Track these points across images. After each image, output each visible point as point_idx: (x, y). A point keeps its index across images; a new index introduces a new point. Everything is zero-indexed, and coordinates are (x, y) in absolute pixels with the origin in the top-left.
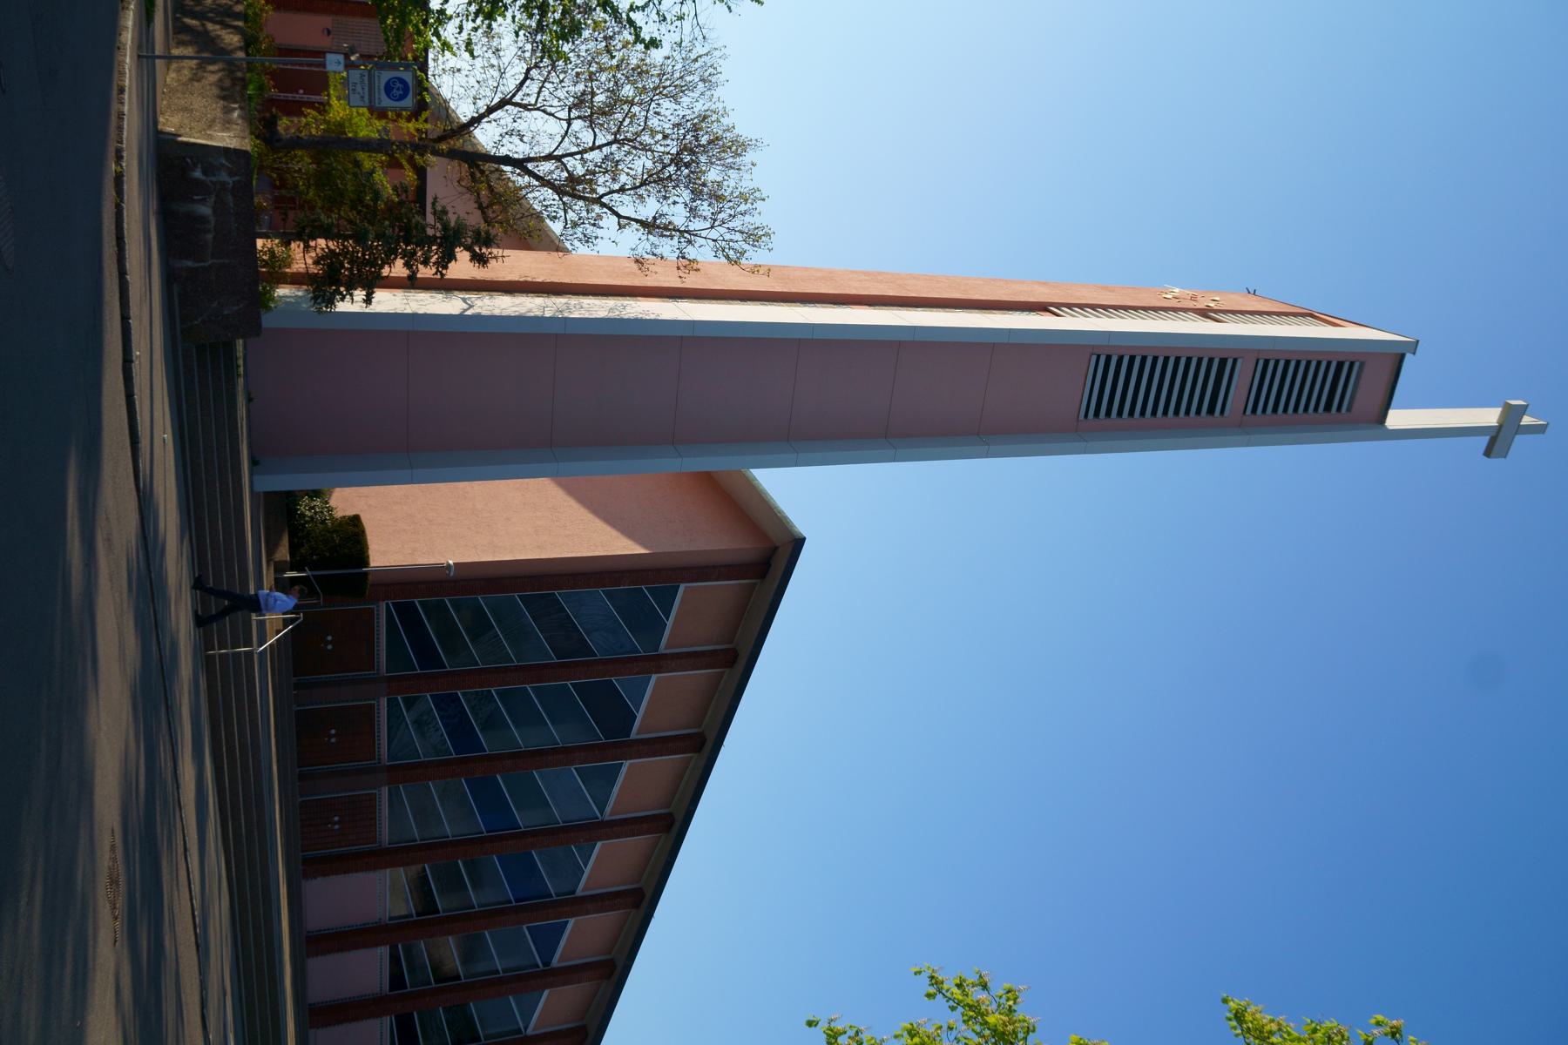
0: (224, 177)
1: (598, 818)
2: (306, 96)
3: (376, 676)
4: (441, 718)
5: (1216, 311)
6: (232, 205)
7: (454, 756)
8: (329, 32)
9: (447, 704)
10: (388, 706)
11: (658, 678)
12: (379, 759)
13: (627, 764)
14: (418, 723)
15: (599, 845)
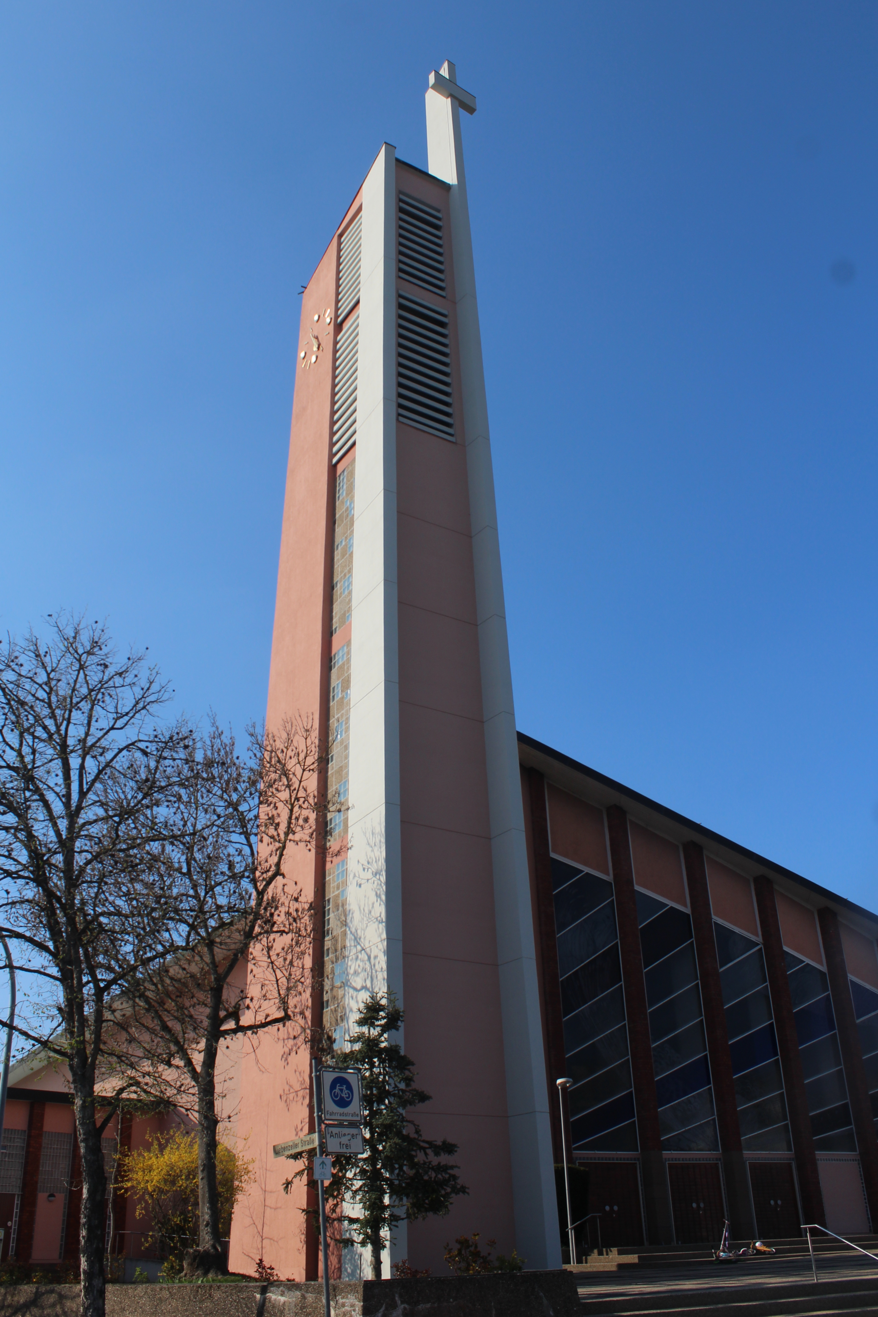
1: (761, 949)
5: (337, 317)
6: (428, 1305)
8: (52, 1195)
10: (670, 1150)
11: (637, 884)
12: (717, 1159)
15: (786, 948)
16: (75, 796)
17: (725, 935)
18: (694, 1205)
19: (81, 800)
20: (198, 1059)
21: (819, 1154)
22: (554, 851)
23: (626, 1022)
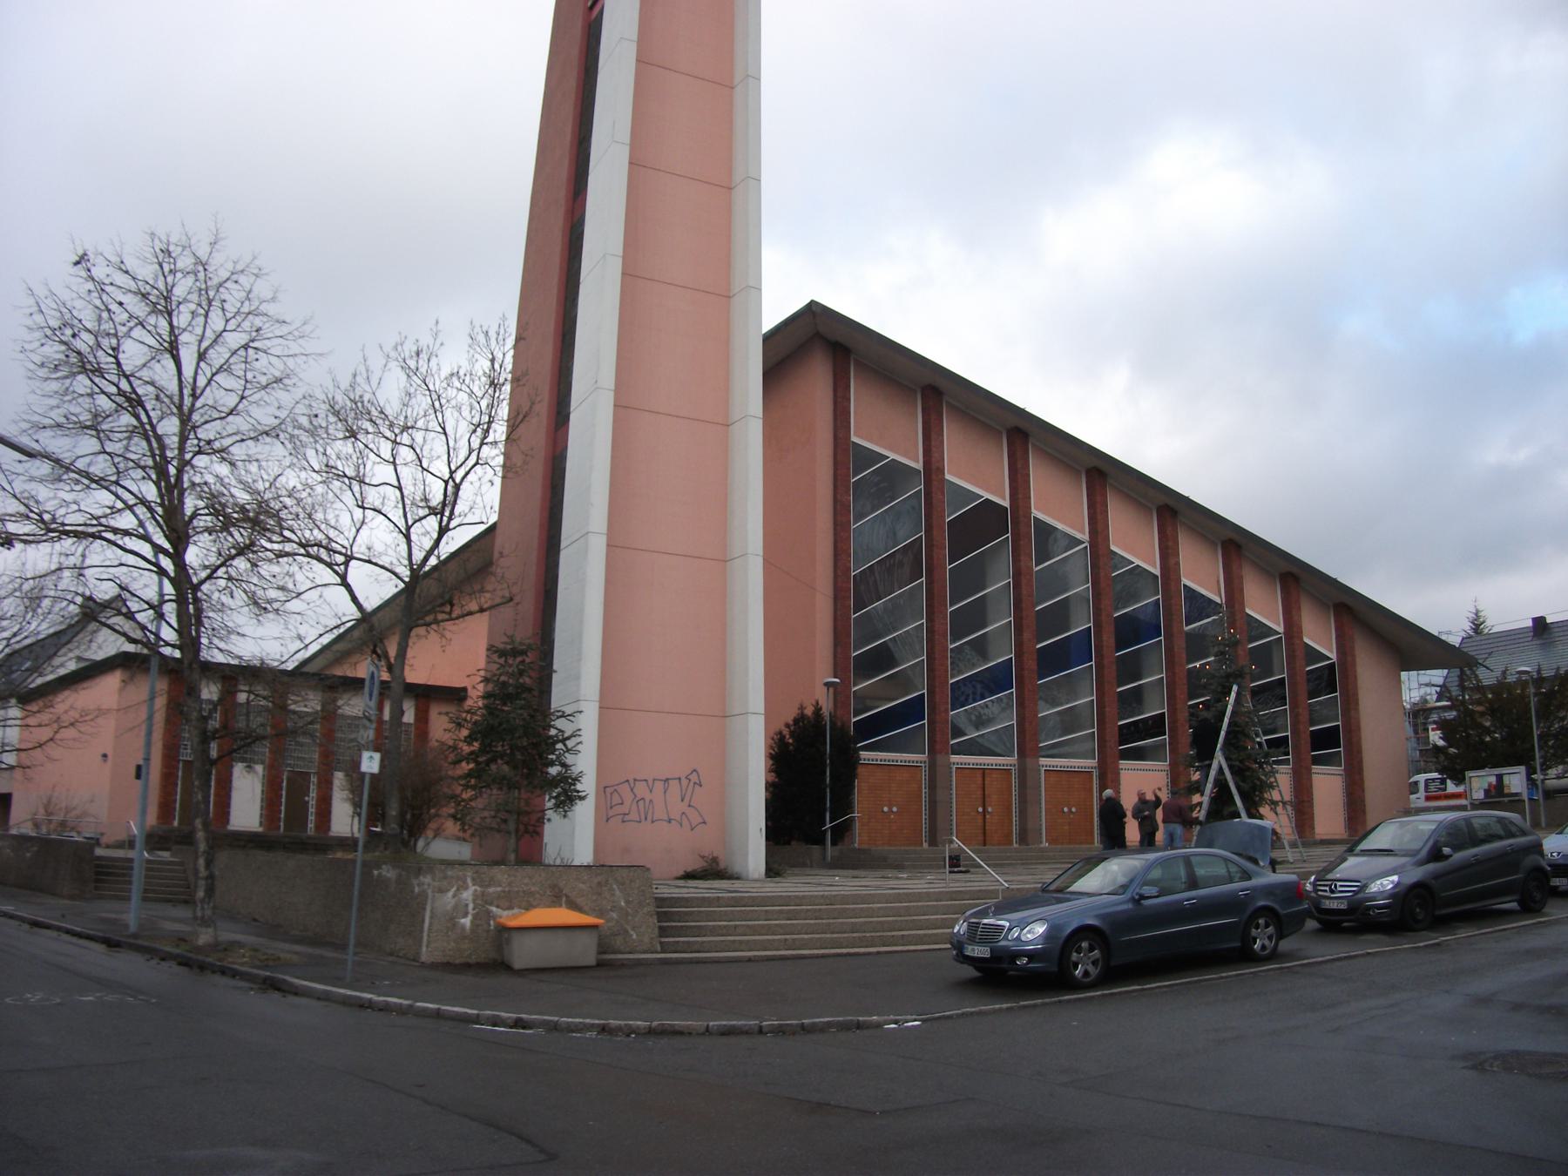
0: (467, 895)
3: (927, 765)
4: (975, 701)
9: (961, 695)
13: (1035, 513)
14: (980, 723)
15: (1113, 548)
16: (187, 401)
17: (1045, 531)
20: (392, 651)
21: (1123, 763)
23: (924, 620)
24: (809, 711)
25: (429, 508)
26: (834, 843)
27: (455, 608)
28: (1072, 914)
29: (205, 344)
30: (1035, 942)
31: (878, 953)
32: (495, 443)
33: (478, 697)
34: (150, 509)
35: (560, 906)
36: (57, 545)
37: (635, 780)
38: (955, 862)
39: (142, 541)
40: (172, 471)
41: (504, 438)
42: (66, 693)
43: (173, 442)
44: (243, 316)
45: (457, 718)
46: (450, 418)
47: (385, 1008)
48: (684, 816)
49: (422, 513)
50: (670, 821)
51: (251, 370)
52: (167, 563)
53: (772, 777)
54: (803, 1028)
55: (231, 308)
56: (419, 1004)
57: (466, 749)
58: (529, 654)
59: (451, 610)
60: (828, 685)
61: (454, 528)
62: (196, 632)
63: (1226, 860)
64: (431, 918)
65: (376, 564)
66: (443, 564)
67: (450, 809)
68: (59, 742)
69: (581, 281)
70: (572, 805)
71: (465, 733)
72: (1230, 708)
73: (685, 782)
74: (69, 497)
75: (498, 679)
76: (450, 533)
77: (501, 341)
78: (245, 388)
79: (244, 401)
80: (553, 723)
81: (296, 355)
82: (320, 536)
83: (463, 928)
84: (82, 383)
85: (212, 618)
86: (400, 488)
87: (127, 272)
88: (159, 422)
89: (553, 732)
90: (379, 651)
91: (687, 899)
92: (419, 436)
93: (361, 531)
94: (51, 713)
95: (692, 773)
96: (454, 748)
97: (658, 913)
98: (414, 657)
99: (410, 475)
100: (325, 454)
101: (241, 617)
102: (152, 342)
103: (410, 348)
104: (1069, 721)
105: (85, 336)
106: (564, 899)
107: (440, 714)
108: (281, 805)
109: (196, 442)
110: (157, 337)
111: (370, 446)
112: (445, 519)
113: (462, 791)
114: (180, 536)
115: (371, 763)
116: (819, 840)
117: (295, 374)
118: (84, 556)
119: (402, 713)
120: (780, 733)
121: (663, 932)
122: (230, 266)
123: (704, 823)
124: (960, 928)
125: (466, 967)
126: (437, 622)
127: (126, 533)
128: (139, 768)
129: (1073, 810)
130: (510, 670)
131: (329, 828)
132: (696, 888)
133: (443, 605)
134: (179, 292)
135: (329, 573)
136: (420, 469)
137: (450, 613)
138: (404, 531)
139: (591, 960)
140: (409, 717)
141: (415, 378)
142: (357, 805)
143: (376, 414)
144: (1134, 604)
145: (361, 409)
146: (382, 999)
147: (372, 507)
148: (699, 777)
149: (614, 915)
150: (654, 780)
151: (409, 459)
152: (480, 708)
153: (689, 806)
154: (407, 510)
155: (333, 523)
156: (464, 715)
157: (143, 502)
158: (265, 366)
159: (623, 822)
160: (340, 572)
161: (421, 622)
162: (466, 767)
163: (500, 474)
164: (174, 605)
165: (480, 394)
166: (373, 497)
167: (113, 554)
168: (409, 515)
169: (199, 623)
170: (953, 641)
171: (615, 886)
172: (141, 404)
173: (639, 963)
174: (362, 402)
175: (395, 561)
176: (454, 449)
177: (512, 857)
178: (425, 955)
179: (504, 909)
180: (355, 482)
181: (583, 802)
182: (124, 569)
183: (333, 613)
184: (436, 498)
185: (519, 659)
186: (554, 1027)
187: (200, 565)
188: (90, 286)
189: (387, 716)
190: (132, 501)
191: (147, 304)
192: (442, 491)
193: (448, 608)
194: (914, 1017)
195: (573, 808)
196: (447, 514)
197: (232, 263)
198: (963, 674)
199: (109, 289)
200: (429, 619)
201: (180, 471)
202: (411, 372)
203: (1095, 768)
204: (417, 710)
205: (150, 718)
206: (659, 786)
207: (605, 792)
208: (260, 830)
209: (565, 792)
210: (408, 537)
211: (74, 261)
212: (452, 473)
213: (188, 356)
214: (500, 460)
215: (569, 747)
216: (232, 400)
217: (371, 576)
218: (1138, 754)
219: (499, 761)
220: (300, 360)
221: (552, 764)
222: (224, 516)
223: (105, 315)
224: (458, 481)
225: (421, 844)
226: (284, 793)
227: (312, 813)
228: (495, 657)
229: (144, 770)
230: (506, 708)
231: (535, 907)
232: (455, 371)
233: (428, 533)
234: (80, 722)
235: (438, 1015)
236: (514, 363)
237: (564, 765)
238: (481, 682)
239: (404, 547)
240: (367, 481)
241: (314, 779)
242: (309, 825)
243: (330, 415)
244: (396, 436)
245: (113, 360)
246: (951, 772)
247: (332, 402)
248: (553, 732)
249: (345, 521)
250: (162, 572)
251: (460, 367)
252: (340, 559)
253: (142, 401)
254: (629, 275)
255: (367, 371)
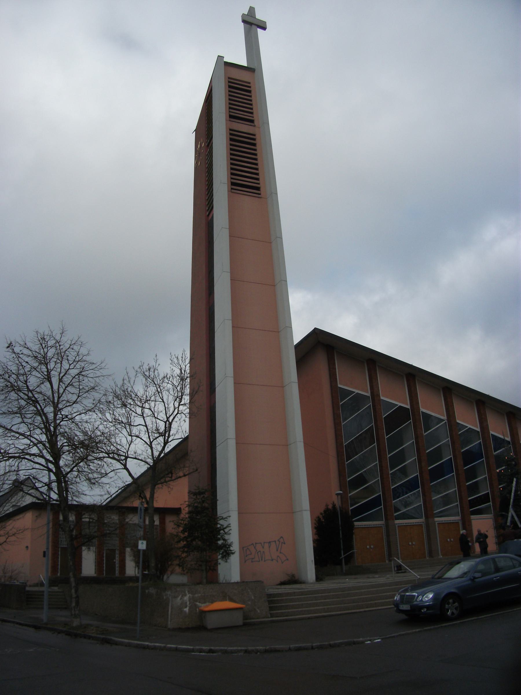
0: (186, 598)
1: (446, 422)
2: (116, 558)
4: (403, 495)
7: (420, 489)
9: (397, 493)
14: (406, 505)
15: (458, 421)
16: (56, 399)
17: (427, 417)
18: (368, 547)
19: (58, 401)
20: (148, 495)
21: (473, 517)
22: (340, 384)
24: (330, 507)
25: (159, 433)
26: (346, 564)
27: (173, 475)
28: (444, 588)
29: (62, 375)
30: (429, 601)
31: (365, 611)
32: (185, 404)
33: (186, 513)
34: (44, 445)
35: (226, 600)
36: (7, 463)
37: (256, 543)
38: (399, 568)
39: (41, 458)
40: (52, 429)
41: (188, 402)
42: (11, 522)
43: (51, 416)
44: (77, 362)
45: (177, 523)
46: (165, 395)
47: (155, 648)
48: (278, 558)
49: (157, 435)
50: (272, 560)
51: (81, 385)
52: (51, 466)
53: (316, 537)
54: (331, 646)
55: (71, 358)
56: (169, 646)
57: (182, 536)
58: (206, 493)
59: (172, 476)
60: (337, 494)
61: (170, 441)
62: (66, 495)
63: (511, 559)
64: (171, 609)
65: (138, 459)
66: (166, 454)
67: (176, 562)
68: (9, 543)
69: (215, 331)
70: (229, 557)
71: (181, 529)
72: (513, 489)
73: (277, 542)
74: (10, 442)
75: (194, 505)
76: (169, 444)
77: (184, 361)
78: (80, 393)
79: (80, 397)
80: (218, 522)
81: (99, 376)
82: (114, 449)
83: (185, 612)
84: (13, 395)
85: (72, 488)
86: (146, 426)
87: (28, 348)
88: (44, 408)
89: (219, 526)
90: (142, 496)
91: (288, 593)
92: (153, 404)
93: (131, 445)
94: (5, 530)
95: (280, 538)
96: (177, 536)
97: (268, 601)
98: (157, 497)
99: (150, 420)
100: (113, 414)
101: (83, 486)
102: (39, 375)
103: (146, 367)
104: (446, 500)
105: (13, 376)
106: (228, 597)
107: (170, 521)
108: (104, 564)
109: (61, 416)
110: (42, 374)
111: (132, 409)
112: (166, 438)
113: (182, 554)
114: (56, 454)
115: (142, 545)
116: (340, 563)
117: (100, 385)
118: (18, 466)
119: (154, 522)
120: (318, 517)
121: (271, 609)
122: (69, 342)
123: (288, 560)
124: (397, 598)
125: (188, 629)
126: (166, 482)
127: (34, 455)
128: (44, 552)
129: (372, 547)
130: (198, 501)
131: (125, 573)
132: (285, 588)
133: (168, 474)
134: (50, 354)
135: (119, 464)
136: (154, 418)
137: (171, 477)
138: (149, 444)
139: (241, 623)
140: (157, 523)
141: (149, 379)
142: (137, 563)
143: (134, 396)
144: (469, 445)
145: (127, 394)
146: (153, 644)
147: (135, 435)
148: (283, 539)
149: (250, 603)
150: (264, 543)
151: (149, 415)
152: (187, 518)
153: (280, 553)
154: (150, 435)
155: (119, 442)
156: (180, 521)
157: (41, 442)
158: (87, 383)
159: (252, 562)
160: (123, 463)
161: (159, 482)
162: (182, 543)
163: (188, 417)
164: (56, 484)
165: (177, 384)
166: (135, 431)
167: (29, 464)
168: (151, 437)
169: (67, 491)
170: (391, 470)
171: (249, 590)
172: (37, 402)
173: (261, 623)
174: (128, 392)
175: (146, 457)
176: (168, 408)
177: (205, 581)
178: (170, 625)
179: (202, 603)
180: (127, 425)
181: (233, 555)
182: (35, 470)
183: (122, 481)
184: (162, 428)
185: (202, 496)
186: (225, 652)
187: (64, 465)
188: (14, 355)
189: (147, 522)
190: (36, 442)
191: (37, 361)
192: (164, 426)
193: (170, 475)
194: (378, 638)
195: (230, 558)
196: (167, 435)
197: (82, 387)
198: (397, 484)
199: (21, 356)
200: (162, 480)
201: (55, 428)
202: (147, 377)
203: (460, 520)
204: (160, 519)
205: (48, 531)
206: (266, 545)
207: (243, 549)
208: (95, 575)
209: (226, 551)
210: (151, 448)
211: (7, 346)
212: (168, 418)
213: (55, 381)
214: (188, 410)
215: (226, 532)
216: (74, 397)
217: (137, 464)
218: (479, 512)
219: (197, 540)
220: (101, 378)
221: (219, 539)
222: (74, 446)
223: (21, 367)
224: (170, 421)
225: (165, 577)
226: (105, 559)
227: (117, 567)
228: (192, 496)
229: (47, 553)
230: (198, 517)
231: (215, 601)
232: (166, 375)
233: (160, 444)
234: (17, 534)
235: (176, 649)
236: (190, 369)
237: (224, 540)
238: (187, 507)
239: (150, 450)
240: (132, 424)
241: (117, 552)
242: (116, 572)
243: (115, 398)
244: (143, 404)
245: (25, 385)
246: (396, 528)
247: (115, 392)
248: (219, 526)
249: (124, 441)
250: (50, 470)
251: (167, 374)
252: (123, 458)
253: (38, 401)
254: (235, 327)
255: (129, 378)
